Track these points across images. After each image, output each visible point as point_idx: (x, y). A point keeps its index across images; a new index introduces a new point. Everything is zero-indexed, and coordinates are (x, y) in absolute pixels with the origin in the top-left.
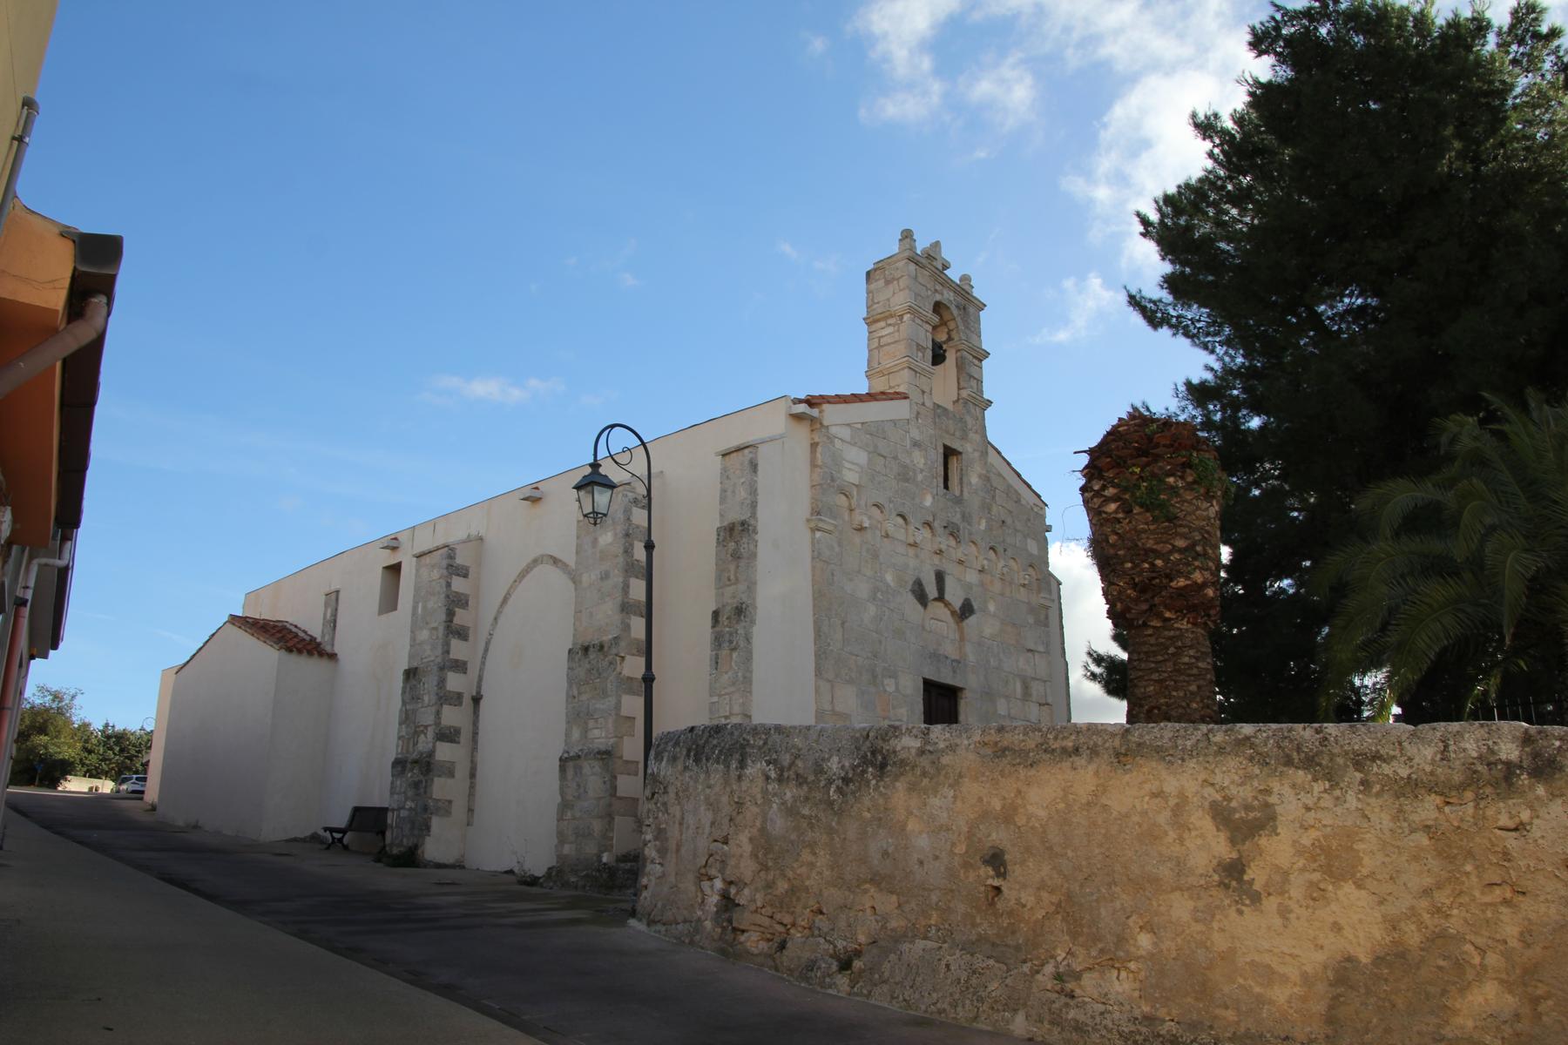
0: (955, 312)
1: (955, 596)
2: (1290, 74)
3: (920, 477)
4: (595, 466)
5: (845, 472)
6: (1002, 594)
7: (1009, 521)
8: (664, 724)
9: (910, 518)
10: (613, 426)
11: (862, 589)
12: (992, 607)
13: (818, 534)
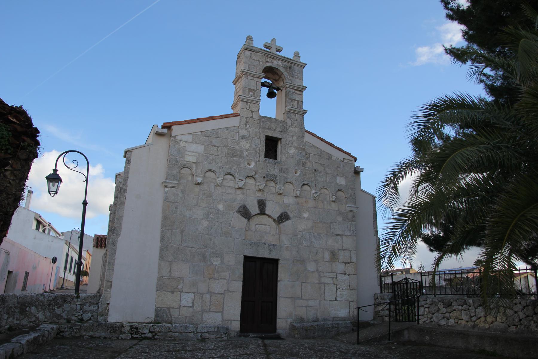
1: (273, 210)
2: (493, 98)
3: (245, 154)
4: (55, 170)
5: (186, 157)
6: (316, 207)
7: (321, 169)
8: (258, 212)
9: (236, 175)
10: (67, 152)
11: (199, 213)
12: (306, 215)
13: (167, 189)
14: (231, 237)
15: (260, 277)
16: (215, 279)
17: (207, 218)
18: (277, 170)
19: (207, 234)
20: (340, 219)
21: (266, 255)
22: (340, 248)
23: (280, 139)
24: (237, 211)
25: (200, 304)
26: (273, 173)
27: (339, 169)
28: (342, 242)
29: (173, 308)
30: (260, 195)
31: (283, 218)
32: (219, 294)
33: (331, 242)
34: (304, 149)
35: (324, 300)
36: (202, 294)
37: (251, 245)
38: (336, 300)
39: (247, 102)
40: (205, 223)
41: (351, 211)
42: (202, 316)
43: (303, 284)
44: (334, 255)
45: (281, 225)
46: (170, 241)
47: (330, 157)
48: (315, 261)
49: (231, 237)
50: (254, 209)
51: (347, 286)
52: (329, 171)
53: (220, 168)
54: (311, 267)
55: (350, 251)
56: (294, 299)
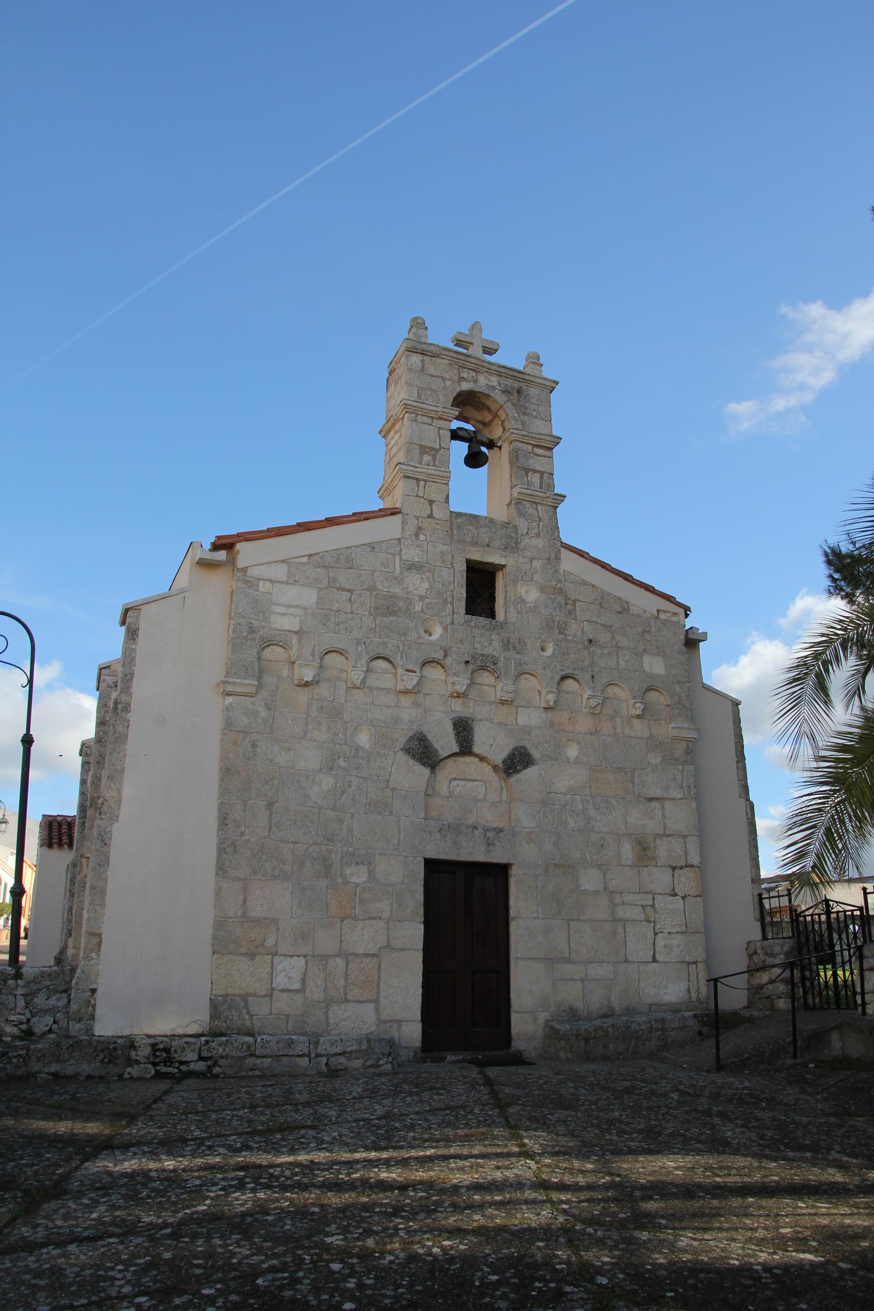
0: (500, 398)
1: (493, 742)
3: (418, 607)
5: (273, 618)
6: (595, 732)
7: (604, 637)
11: (310, 759)
15: (465, 907)
16: (355, 919)
17: (331, 768)
18: (496, 644)
19: (333, 809)
20: (655, 759)
24: (402, 749)
29: (255, 995)
31: (517, 761)
32: (367, 955)
33: (637, 818)
34: (561, 591)
35: (626, 961)
37: (440, 831)
38: (654, 960)
39: (418, 480)
40: (327, 781)
41: (682, 739)
42: (326, 1013)
43: (573, 924)
44: (644, 849)
47: (624, 608)
48: (599, 866)
49: (391, 813)
50: (445, 742)
51: (680, 926)
52: (624, 642)
53: (358, 643)
54: (590, 880)
55: (684, 837)
56: (551, 961)
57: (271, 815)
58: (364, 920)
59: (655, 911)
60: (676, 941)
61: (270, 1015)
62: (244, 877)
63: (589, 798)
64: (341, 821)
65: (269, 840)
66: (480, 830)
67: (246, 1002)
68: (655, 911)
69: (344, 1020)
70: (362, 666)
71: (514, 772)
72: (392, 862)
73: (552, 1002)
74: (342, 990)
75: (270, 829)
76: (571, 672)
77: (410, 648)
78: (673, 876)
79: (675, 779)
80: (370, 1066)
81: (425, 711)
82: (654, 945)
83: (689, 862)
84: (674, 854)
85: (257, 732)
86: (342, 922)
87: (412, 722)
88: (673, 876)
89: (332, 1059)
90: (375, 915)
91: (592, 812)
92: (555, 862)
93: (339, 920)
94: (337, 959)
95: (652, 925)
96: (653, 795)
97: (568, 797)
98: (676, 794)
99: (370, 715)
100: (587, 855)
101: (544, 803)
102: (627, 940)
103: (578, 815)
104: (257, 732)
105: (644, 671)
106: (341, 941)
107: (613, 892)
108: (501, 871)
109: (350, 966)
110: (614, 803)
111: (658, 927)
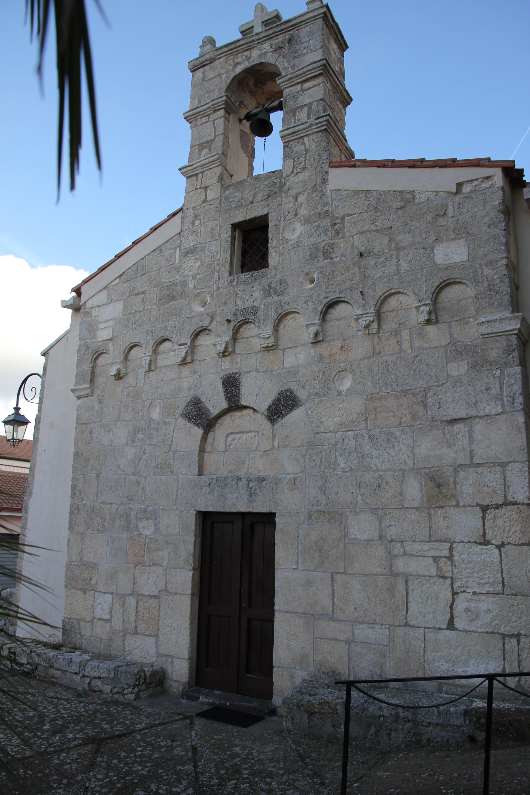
1: (258, 392)
4: (17, 409)
6: (375, 354)
10: (25, 381)
11: (121, 435)
14: (172, 472)
15: (234, 556)
16: (144, 565)
17: (134, 441)
18: (257, 294)
19: (134, 474)
20: (458, 368)
21: (242, 508)
22: (463, 459)
23: (267, 215)
24: (181, 415)
25: (120, 615)
26: (250, 303)
27: (442, 221)
28: (471, 440)
29: (84, 620)
30: (227, 366)
31: (283, 405)
32: (151, 596)
33: (430, 448)
34: (327, 214)
35: (407, 624)
36: (123, 596)
37: (209, 485)
38: (451, 625)
39: (197, 175)
40: (131, 452)
41: (498, 335)
42: (124, 641)
43: (338, 578)
44: (439, 486)
45: (278, 425)
46: (83, 496)
47: (406, 199)
48: (374, 511)
49: (172, 472)
50: (216, 402)
51: (492, 585)
52: (406, 239)
53: (147, 334)
54: (362, 527)
55: (503, 465)
56: (311, 617)
57: (98, 483)
58: (150, 566)
59: (453, 564)
60: (486, 604)
61: (91, 636)
62: (82, 532)
63: (364, 432)
64: (138, 483)
65: (96, 503)
66: (244, 481)
67: (79, 624)
68: (453, 564)
69: (135, 649)
70: (149, 351)
71: (278, 417)
72: (171, 516)
73: (311, 661)
74: (133, 624)
75: (97, 494)
76: (337, 296)
77: (183, 325)
78: (483, 518)
79: (488, 389)
80: (116, 693)
81: (200, 376)
82: (451, 607)
83: (510, 499)
84: (485, 489)
85: (93, 422)
86: (135, 567)
87: (189, 389)
88: (483, 518)
89: (93, 681)
90: (157, 562)
91: (367, 448)
92: (320, 508)
93: (133, 566)
94: (131, 598)
95: (448, 581)
96: (454, 415)
97: (339, 434)
98: (493, 408)
99: (160, 391)
100: (359, 499)
101: (310, 445)
102: (410, 598)
103: (349, 453)
104: (93, 422)
105: (436, 264)
106: (134, 584)
107: (392, 541)
108: (268, 519)
109: (139, 605)
110: (397, 433)
111: (456, 585)
